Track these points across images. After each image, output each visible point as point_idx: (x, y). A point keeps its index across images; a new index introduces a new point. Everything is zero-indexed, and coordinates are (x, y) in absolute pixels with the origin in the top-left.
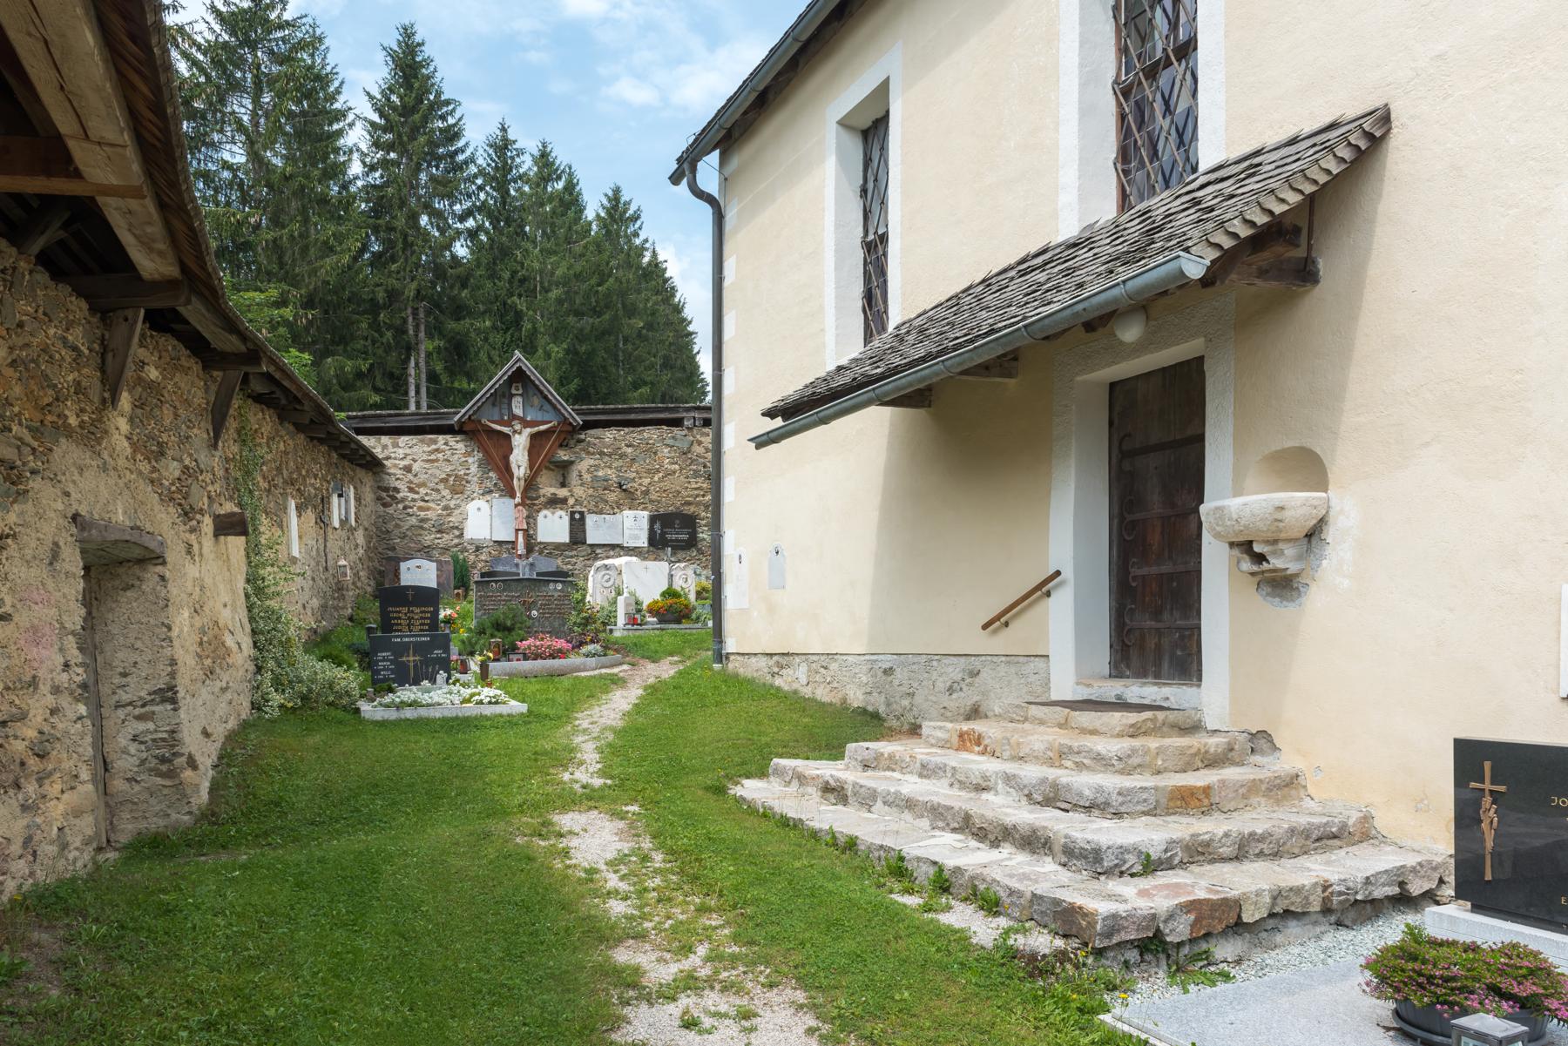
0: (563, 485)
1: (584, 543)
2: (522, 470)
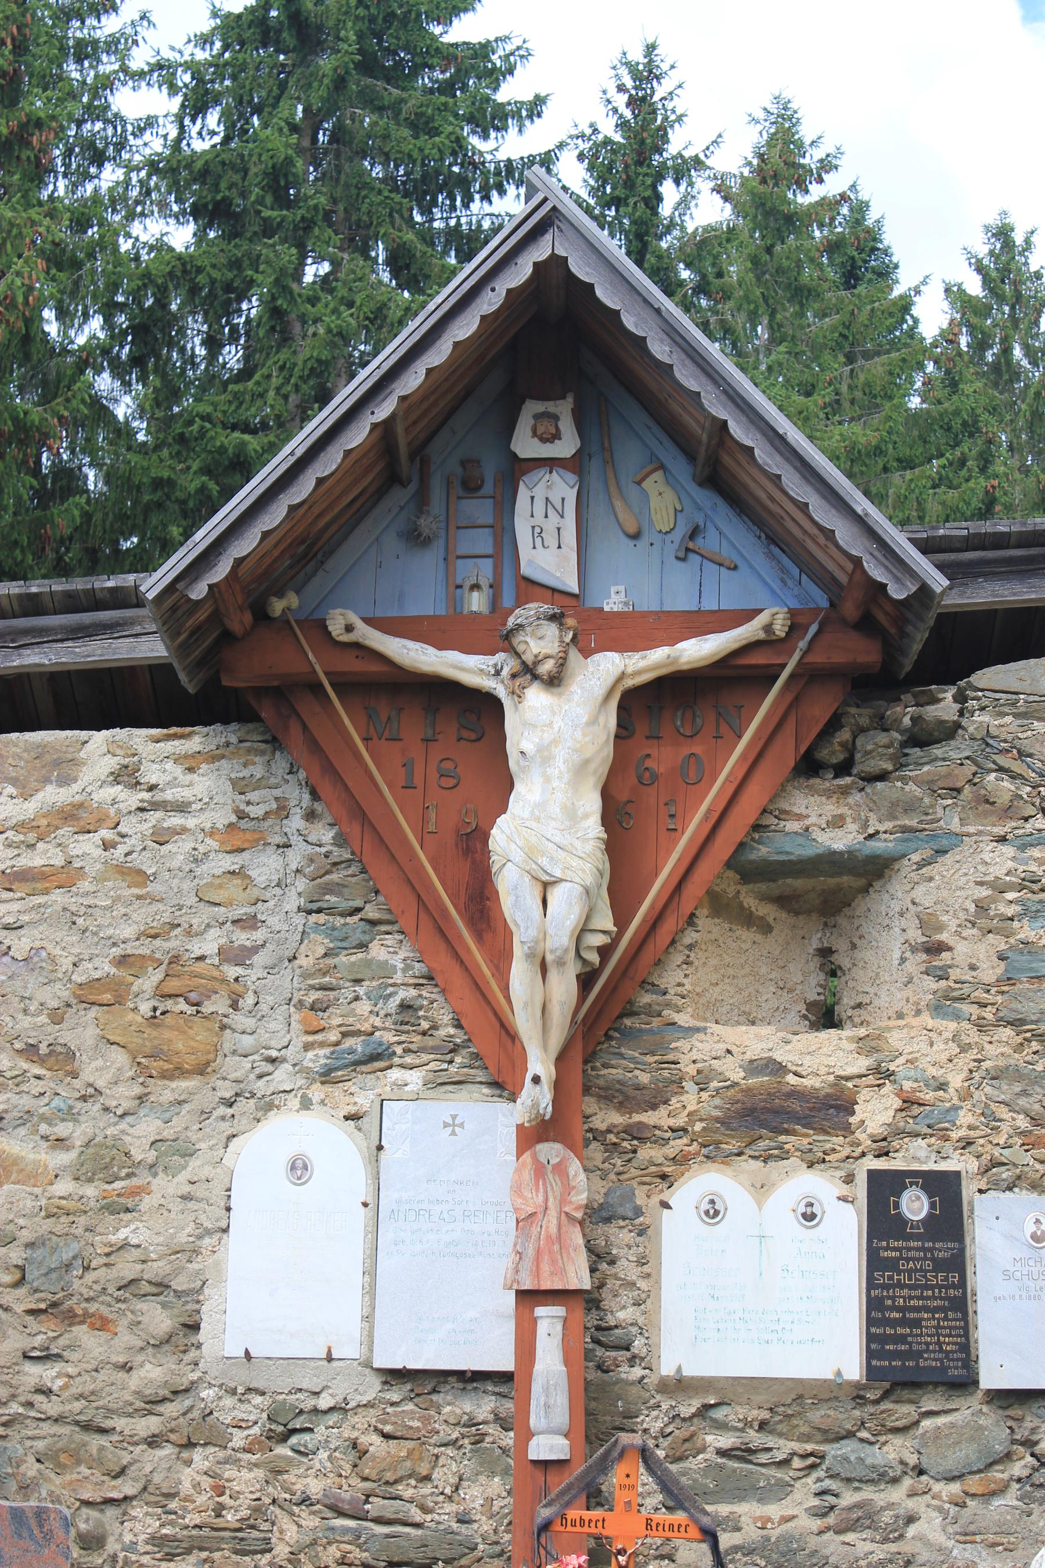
0: (825, 1017)
1: (963, 1382)
2: (566, 908)
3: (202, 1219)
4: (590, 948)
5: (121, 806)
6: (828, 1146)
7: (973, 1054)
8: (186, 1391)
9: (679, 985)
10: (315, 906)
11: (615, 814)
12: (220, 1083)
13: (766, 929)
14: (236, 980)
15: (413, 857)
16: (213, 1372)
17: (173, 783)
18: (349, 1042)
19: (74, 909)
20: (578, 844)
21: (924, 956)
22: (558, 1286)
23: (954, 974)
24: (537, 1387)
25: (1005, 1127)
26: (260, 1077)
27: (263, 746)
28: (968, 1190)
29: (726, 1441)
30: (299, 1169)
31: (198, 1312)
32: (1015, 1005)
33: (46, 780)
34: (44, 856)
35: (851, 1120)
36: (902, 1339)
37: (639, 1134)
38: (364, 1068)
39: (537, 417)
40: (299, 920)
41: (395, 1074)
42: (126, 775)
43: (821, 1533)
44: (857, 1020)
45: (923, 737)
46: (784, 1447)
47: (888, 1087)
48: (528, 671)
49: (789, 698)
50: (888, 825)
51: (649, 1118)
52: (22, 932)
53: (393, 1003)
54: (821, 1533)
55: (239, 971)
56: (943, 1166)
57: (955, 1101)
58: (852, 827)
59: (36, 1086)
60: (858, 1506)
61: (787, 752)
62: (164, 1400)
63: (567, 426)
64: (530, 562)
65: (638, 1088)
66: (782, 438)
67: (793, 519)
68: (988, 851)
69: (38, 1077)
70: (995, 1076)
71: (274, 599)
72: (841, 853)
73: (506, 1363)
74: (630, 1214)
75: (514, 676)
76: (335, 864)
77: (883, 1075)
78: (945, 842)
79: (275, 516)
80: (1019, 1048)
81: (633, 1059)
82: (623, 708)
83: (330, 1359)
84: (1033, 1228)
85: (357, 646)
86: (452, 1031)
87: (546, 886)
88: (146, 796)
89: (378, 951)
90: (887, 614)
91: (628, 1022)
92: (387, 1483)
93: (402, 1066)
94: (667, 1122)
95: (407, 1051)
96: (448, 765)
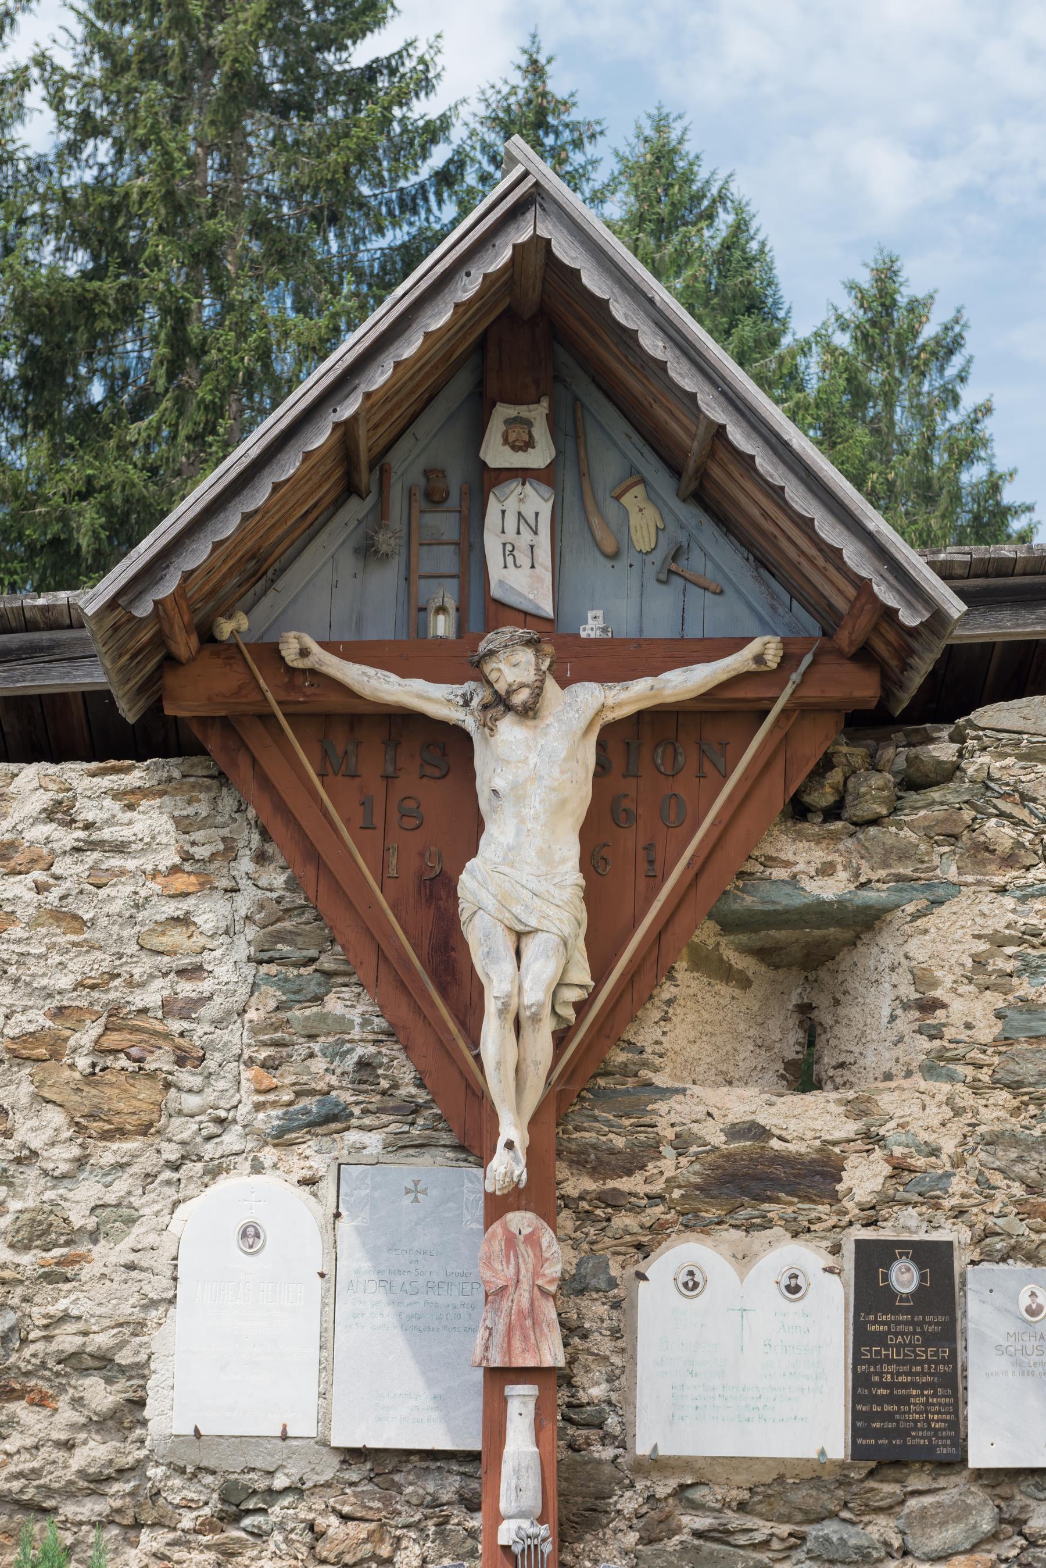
3: (147, 1289)
4: (566, 1003)
6: (814, 1215)
7: (967, 1118)
8: (132, 1469)
9: (657, 1043)
10: (265, 956)
11: (592, 861)
12: (164, 1145)
13: (744, 982)
14: (182, 1035)
15: (374, 903)
17: (111, 822)
18: (304, 1102)
20: (555, 891)
21: (917, 1014)
22: (531, 1363)
23: (949, 1033)
24: (506, 1470)
25: (1000, 1196)
26: (209, 1138)
27: (208, 782)
28: (960, 1260)
29: (702, 1522)
31: (143, 1387)
32: (1011, 1066)
35: (838, 1187)
36: (889, 1416)
37: (613, 1201)
38: (320, 1130)
39: (509, 422)
40: (249, 970)
41: (353, 1137)
42: (59, 812)
44: (839, 1080)
45: (915, 781)
46: (763, 1529)
47: (878, 1153)
48: (500, 703)
49: (780, 734)
50: (882, 873)
51: (624, 1184)
53: (352, 1059)
55: (186, 1025)
56: (935, 1236)
57: (948, 1168)
58: (842, 875)
61: (775, 794)
62: (109, 1479)
63: (541, 432)
64: (501, 583)
65: (612, 1152)
66: (786, 445)
67: (789, 538)
68: (986, 900)
70: (991, 1141)
71: (221, 620)
72: (831, 903)
73: (474, 1444)
74: (603, 1285)
75: (485, 707)
76: (287, 911)
77: (872, 1139)
78: (941, 892)
79: (228, 526)
80: (1015, 1112)
81: (607, 1123)
83: (284, 1437)
85: (313, 672)
86: (414, 1091)
88: (82, 834)
89: (334, 1005)
90: (888, 643)
91: (601, 1082)
93: (360, 1128)
94: (643, 1189)
95: (365, 1112)
96: (411, 804)
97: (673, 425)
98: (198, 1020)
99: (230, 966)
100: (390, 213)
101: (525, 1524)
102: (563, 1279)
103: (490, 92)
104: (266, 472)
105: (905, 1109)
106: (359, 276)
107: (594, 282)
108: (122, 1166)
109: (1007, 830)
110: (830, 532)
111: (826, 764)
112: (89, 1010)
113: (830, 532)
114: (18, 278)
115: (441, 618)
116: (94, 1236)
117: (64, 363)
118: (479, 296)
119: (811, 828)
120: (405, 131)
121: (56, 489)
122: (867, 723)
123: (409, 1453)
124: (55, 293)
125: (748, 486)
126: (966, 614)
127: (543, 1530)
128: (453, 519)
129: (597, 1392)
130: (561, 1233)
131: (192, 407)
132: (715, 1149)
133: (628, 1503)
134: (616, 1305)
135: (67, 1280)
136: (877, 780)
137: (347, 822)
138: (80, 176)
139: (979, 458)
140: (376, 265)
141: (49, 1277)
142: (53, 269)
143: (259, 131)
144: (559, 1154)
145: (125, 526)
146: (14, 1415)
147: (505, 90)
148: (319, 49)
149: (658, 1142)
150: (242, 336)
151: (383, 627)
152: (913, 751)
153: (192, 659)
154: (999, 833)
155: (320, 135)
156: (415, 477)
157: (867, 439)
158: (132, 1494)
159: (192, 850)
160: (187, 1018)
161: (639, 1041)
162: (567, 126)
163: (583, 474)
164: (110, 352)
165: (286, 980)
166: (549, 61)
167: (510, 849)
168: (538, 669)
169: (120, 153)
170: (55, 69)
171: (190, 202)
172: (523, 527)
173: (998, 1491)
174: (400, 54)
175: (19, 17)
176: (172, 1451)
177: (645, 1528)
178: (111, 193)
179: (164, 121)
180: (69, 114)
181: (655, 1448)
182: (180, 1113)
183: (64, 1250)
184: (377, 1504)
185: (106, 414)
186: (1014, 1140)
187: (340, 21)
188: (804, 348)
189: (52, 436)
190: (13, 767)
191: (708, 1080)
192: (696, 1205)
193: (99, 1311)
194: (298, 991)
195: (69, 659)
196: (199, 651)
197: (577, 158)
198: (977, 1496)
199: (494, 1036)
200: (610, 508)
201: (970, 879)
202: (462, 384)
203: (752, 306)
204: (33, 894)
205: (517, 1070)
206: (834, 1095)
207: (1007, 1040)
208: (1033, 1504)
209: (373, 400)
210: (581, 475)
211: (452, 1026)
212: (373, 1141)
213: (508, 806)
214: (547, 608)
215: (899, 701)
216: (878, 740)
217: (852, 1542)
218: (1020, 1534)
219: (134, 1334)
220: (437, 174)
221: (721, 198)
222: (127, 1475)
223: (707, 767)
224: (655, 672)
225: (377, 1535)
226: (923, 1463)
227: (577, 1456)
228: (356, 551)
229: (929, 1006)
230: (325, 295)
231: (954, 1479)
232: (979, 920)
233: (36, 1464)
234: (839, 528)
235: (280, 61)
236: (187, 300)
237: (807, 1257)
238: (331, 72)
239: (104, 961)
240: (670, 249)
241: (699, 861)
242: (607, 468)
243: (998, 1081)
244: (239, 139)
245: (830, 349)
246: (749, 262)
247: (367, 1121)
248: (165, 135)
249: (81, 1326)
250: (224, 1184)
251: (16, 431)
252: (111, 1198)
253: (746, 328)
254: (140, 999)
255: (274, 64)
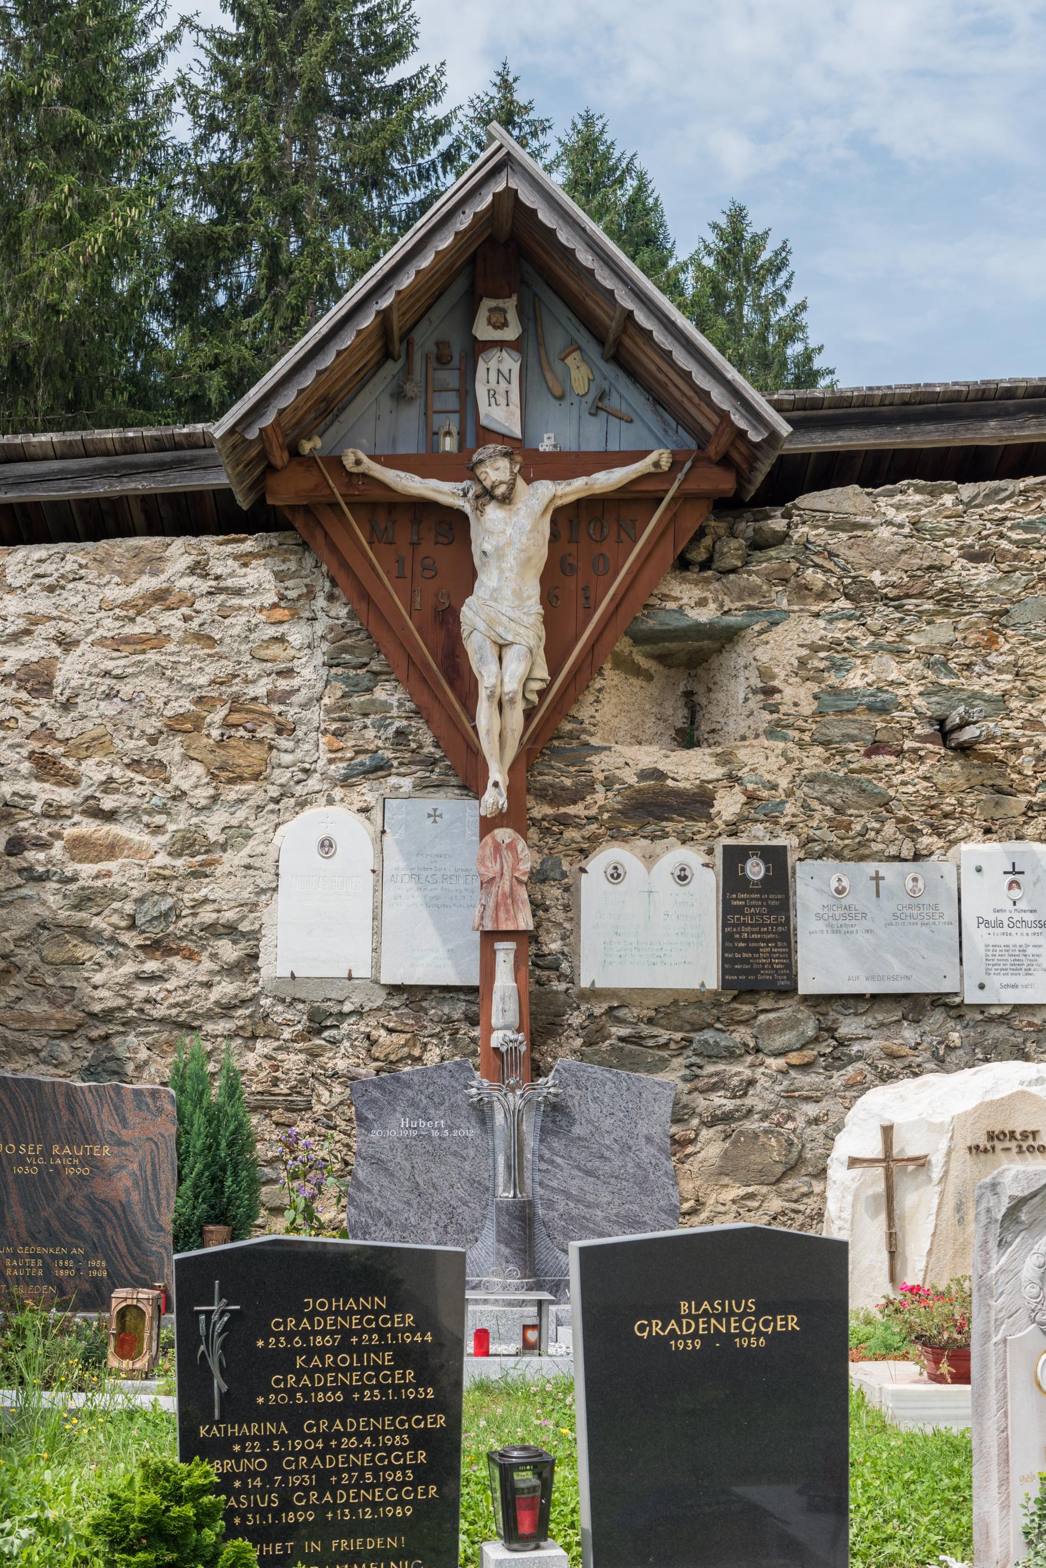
1: (790, 991)
3: (259, 881)
4: (532, 691)
5: (196, 591)
6: (696, 829)
7: (796, 765)
8: (250, 1000)
9: (592, 717)
10: (335, 662)
11: (549, 597)
12: (269, 787)
13: (649, 677)
14: (280, 714)
15: (405, 626)
16: (269, 987)
17: (232, 575)
18: (361, 758)
19: (164, 664)
20: (525, 618)
21: (762, 697)
22: (511, 927)
23: (783, 709)
24: (496, 998)
25: (817, 816)
26: (298, 782)
27: (296, 548)
28: (792, 858)
29: (624, 1032)
30: (327, 846)
31: (257, 946)
32: (824, 731)
33: (142, 572)
34: (142, 626)
35: (712, 811)
36: (746, 961)
37: (565, 821)
38: (371, 776)
39: (490, 310)
40: (324, 671)
41: (393, 780)
42: (198, 569)
43: (690, 1093)
44: (711, 741)
45: (759, 544)
46: (664, 1035)
47: (737, 788)
48: (487, 494)
49: (670, 514)
50: (738, 605)
51: (571, 810)
52: (127, 680)
53: (391, 730)
54: (690, 1093)
55: (283, 708)
56: (775, 842)
57: (783, 797)
58: (712, 606)
59: (139, 790)
60: (717, 1074)
61: (668, 553)
62: (235, 1007)
63: (512, 317)
64: (487, 415)
65: (563, 789)
66: (673, 323)
67: (676, 385)
68: (806, 622)
69: (141, 783)
70: (811, 780)
71: (304, 441)
72: (705, 624)
73: (475, 981)
74: (558, 877)
75: (477, 497)
76: (348, 632)
77: (733, 779)
78: (777, 616)
79: (307, 379)
80: (827, 760)
81: (560, 770)
82: (553, 522)
83: (350, 978)
84: (836, 884)
85: (364, 475)
86: (433, 750)
87: (501, 647)
88: (213, 583)
89: (380, 694)
90: (741, 453)
91: (556, 743)
92: (391, 1062)
93: (398, 774)
94: (583, 813)
95: (401, 764)
96: (428, 561)
97: (599, 312)
98: (290, 705)
99: (311, 669)
100: (412, 180)
101: (509, 1033)
102: (531, 872)
103: (476, 101)
104: (332, 343)
105: (757, 759)
106: (392, 221)
107: (546, 217)
108: (242, 801)
109: (820, 576)
110: (703, 380)
111: (701, 533)
112: (220, 699)
113: (703, 380)
114: (169, 224)
115: (448, 439)
116: (224, 847)
117: (199, 280)
118: (471, 227)
119: (692, 575)
120: (421, 126)
121: (194, 362)
122: (728, 506)
123: (432, 988)
124: (193, 234)
125: (649, 351)
126: (791, 434)
127: (520, 1037)
128: (456, 374)
129: (555, 946)
130: (530, 843)
131: (283, 308)
132: (631, 786)
133: (576, 1019)
134: (567, 889)
135: (207, 876)
136: (734, 544)
137: (387, 573)
138: (209, 157)
139: (799, 339)
140: (403, 214)
141: (195, 874)
142: (192, 218)
143: (326, 128)
144: (528, 791)
145: (237, 388)
146: (173, 965)
147: (486, 99)
148: (364, 73)
149: (593, 783)
150: (315, 261)
151: (410, 445)
152: (758, 524)
153: (285, 467)
154: (814, 577)
155: (366, 130)
156: (430, 347)
157: (725, 327)
158: (250, 1016)
159: (286, 593)
160: (283, 703)
161: (581, 715)
162: (527, 123)
163: (540, 343)
164: (229, 273)
165: (348, 678)
166: (515, 80)
167: (495, 590)
168: (512, 472)
169: (235, 141)
170: (191, 87)
171: (281, 174)
172: (501, 379)
173: (818, 1009)
174: (417, 75)
175: (168, 53)
176: (277, 988)
177: (587, 1036)
178: (230, 169)
179: (263, 121)
180: (201, 117)
181: (593, 983)
182: (279, 766)
183: (204, 857)
184: (411, 1022)
185: (226, 313)
186: (826, 779)
187: (377, 55)
188: (683, 268)
189: (192, 328)
190: (168, 540)
191: (626, 744)
192: (619, 823)
193: (227, 896)
194: (356, 685)
195: (204, 468)
196: (289, 462)
197: (534, 144)
198: (804, 1013)
199: (485, 715)
200: (558, 366)
201: (796, 608)
202: (460, 286)
203: (650, 240)
204: (181, 623)
205: (500, 735)
206: (708, 751)
207: (821, 713)
208: (841, 1018)
209: (403, 295)
210: (539, 344)
211: (457, 707)
212: (407, 783)
213: (493, 563)
214: (517, 432)
215: (749, 492)
216: (735, 518)
217: (723, 1043)
218: (833, 1038)
219: (251, 911)
220: (442, 154)
221: (628, 170)
222: (247, 1004)
223: (623, 536)
224: (588, 474)
225: (411, 1043)
226: (769, 991)
227: (542, 989)
228: (392, 395)
229: (770, 691)
230: (370, 235)
231: (789, 1002)
232: (802, 635)
233: (187, 998)
234: (708, 378)
235: (339, 82)
236: (279, 238)
237: (691, 856)
238: (372, 88)
239: (228, 666)
240: (595, 202)
241: (619, 597)
242: (556, 340)
243: (815, 741)
244: (312, 132)
245: (700, 267)
246: (647, 211)
247: (402, 770)
248: (265, 130)
249: (216, 906)
250: (308, 812)
251: (168, 325)
252: (234, 822)
253: (645, 255)
254: (252, 691)
255: (335, 83)
